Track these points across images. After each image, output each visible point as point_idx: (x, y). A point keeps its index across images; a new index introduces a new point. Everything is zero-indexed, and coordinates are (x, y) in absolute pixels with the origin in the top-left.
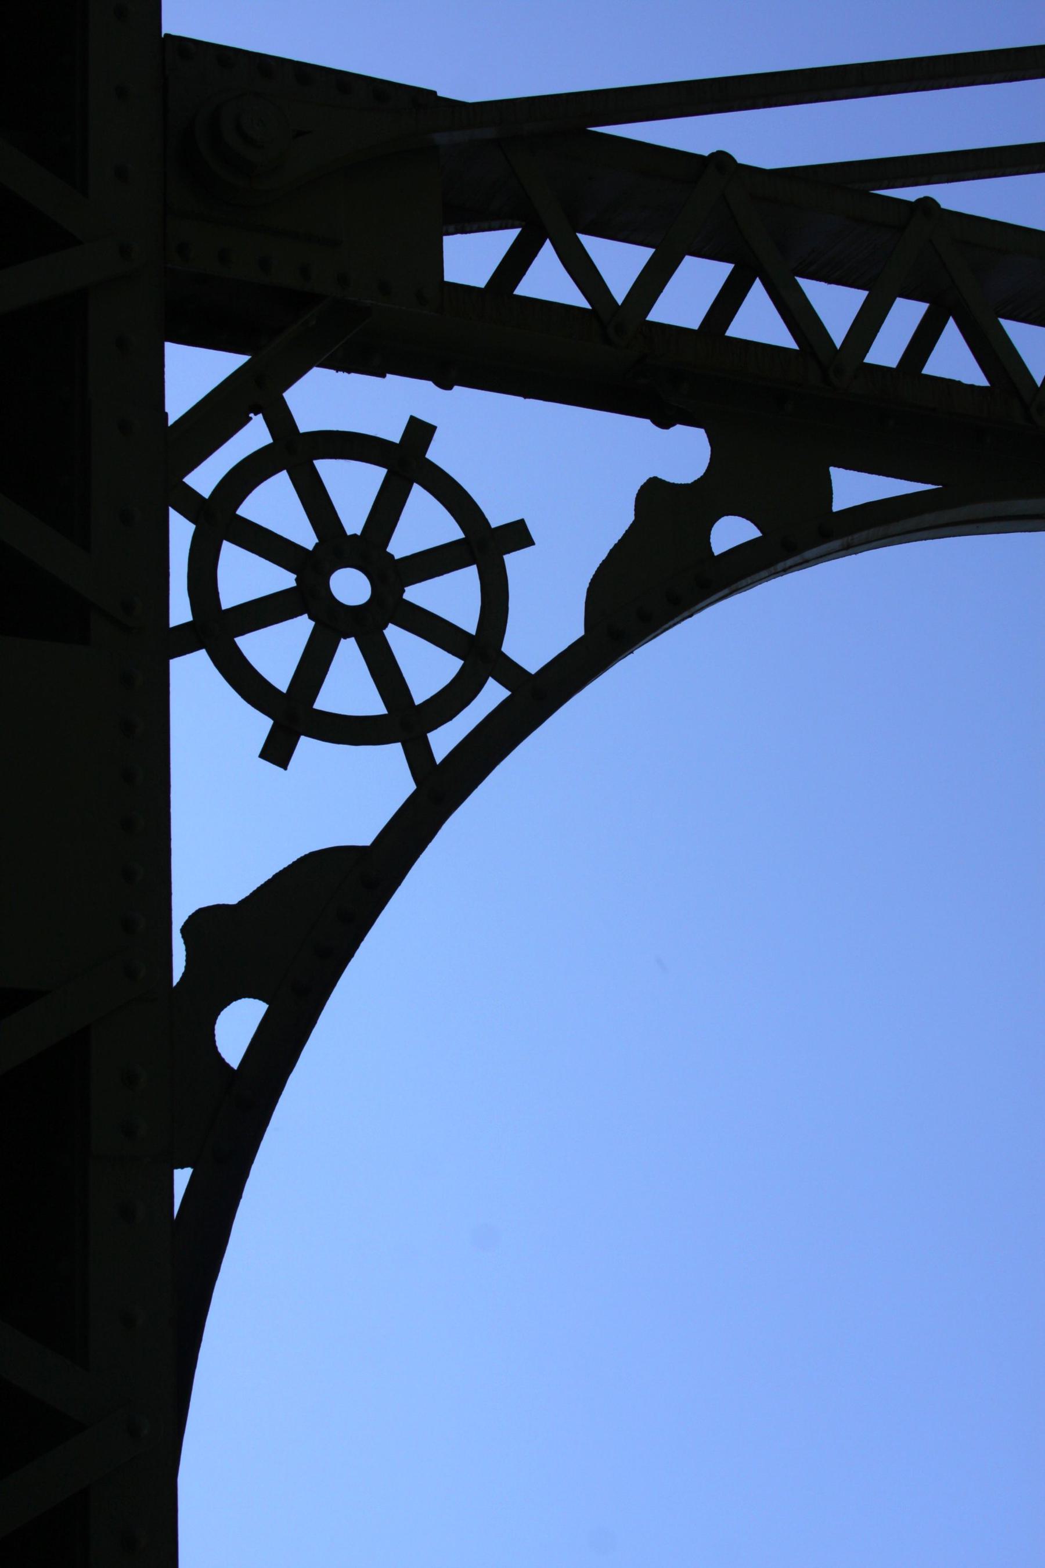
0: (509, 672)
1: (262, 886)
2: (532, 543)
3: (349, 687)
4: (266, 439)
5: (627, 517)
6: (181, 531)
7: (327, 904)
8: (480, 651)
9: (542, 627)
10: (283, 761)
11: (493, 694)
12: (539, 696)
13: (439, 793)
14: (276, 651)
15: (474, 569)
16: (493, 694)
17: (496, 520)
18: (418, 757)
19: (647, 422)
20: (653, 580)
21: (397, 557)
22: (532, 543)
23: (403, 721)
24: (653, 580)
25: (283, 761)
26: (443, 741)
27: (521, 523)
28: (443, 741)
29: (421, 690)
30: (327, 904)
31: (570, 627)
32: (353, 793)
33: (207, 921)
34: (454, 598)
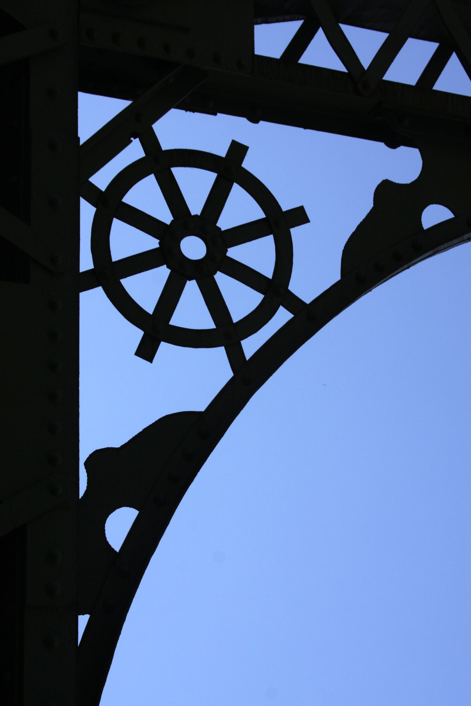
0: (293, 303)
2: (151, 362)
8: (275, 290)
9: (312, 277)
11: (282, 316)
12: (311, 318)
14: (259, 255)
16: (282, 316)
18: (235, 355)
19: (117, 443)
20: (384, 245)
21: (223, 229)
22: (151, 362)
23: (226, 333)
24: (384, 245)
26: (251, 345)
29: (237, 315)
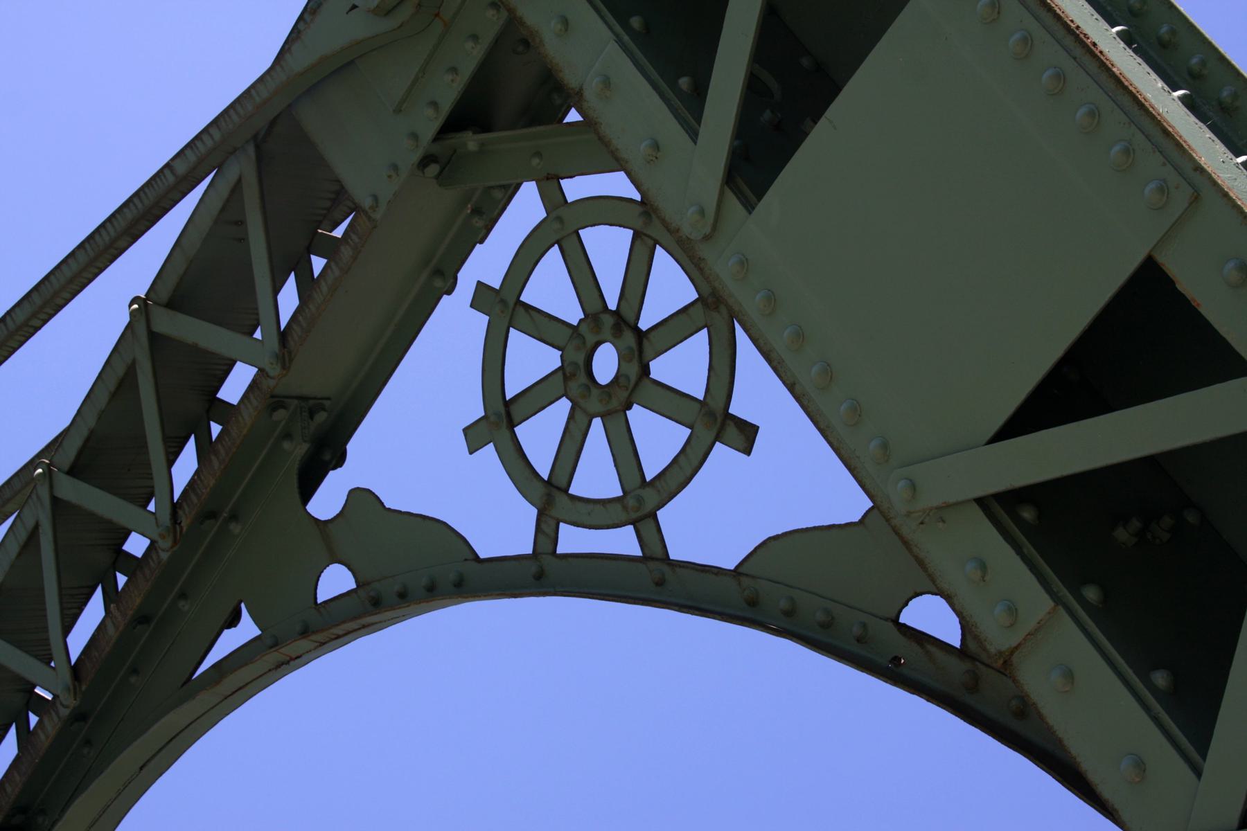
1: (430, 314)
3: (540, 437)
4: (256, 632)
5: (351, 447)
6: (525, 209)
7: (420, 569)
8: (641, 501)
10: (474, 447)
12: (658, 581)
13: (540, 574)
14: (657, 439)
15: (491, 446)
17: (738, 408)
23: (551, 496)
25: (474, 447)
26: (573, 540)
27: (755, 429)
28: (573, 540)
30: (420, 569)
31: (726, 554)
32: (498, 522)
33: (361, 499)
34: (657, 439)
